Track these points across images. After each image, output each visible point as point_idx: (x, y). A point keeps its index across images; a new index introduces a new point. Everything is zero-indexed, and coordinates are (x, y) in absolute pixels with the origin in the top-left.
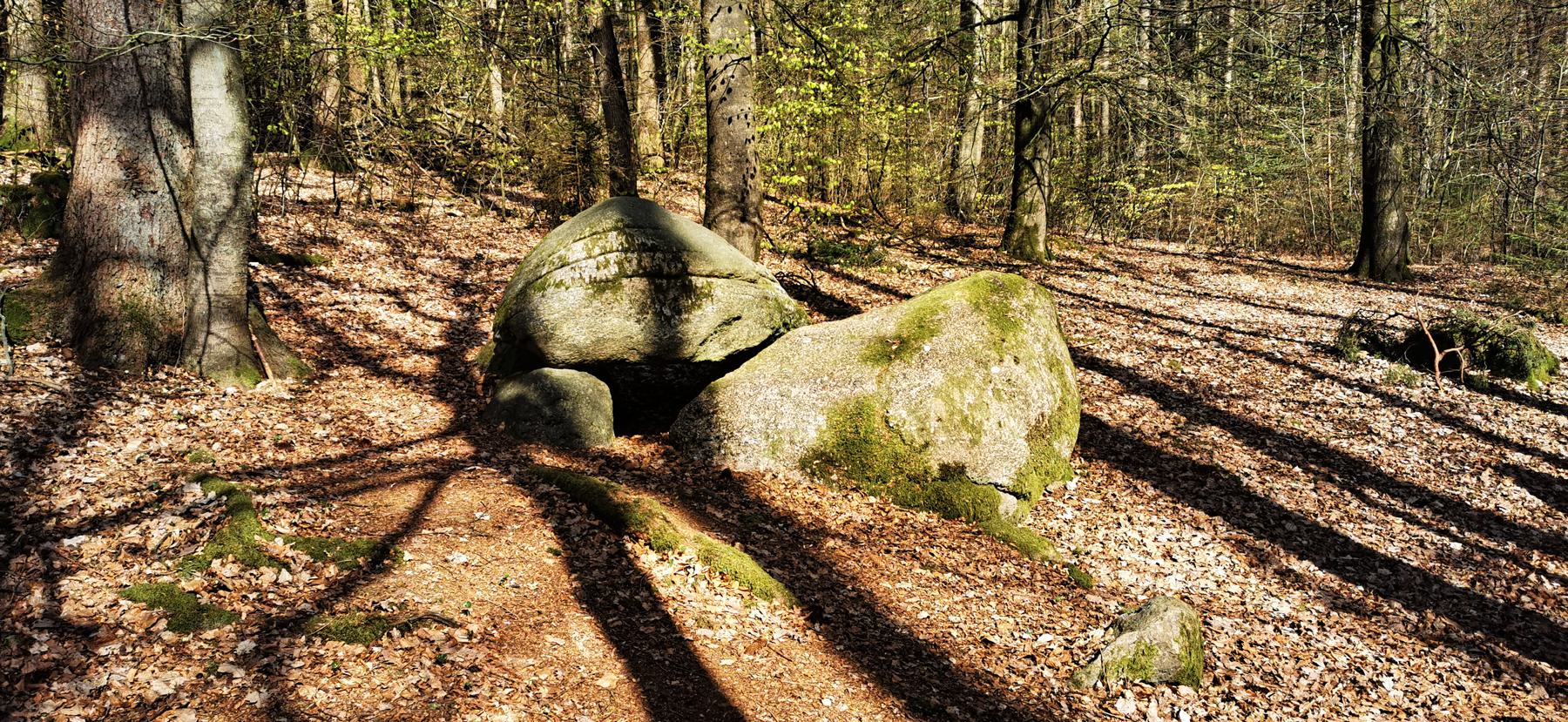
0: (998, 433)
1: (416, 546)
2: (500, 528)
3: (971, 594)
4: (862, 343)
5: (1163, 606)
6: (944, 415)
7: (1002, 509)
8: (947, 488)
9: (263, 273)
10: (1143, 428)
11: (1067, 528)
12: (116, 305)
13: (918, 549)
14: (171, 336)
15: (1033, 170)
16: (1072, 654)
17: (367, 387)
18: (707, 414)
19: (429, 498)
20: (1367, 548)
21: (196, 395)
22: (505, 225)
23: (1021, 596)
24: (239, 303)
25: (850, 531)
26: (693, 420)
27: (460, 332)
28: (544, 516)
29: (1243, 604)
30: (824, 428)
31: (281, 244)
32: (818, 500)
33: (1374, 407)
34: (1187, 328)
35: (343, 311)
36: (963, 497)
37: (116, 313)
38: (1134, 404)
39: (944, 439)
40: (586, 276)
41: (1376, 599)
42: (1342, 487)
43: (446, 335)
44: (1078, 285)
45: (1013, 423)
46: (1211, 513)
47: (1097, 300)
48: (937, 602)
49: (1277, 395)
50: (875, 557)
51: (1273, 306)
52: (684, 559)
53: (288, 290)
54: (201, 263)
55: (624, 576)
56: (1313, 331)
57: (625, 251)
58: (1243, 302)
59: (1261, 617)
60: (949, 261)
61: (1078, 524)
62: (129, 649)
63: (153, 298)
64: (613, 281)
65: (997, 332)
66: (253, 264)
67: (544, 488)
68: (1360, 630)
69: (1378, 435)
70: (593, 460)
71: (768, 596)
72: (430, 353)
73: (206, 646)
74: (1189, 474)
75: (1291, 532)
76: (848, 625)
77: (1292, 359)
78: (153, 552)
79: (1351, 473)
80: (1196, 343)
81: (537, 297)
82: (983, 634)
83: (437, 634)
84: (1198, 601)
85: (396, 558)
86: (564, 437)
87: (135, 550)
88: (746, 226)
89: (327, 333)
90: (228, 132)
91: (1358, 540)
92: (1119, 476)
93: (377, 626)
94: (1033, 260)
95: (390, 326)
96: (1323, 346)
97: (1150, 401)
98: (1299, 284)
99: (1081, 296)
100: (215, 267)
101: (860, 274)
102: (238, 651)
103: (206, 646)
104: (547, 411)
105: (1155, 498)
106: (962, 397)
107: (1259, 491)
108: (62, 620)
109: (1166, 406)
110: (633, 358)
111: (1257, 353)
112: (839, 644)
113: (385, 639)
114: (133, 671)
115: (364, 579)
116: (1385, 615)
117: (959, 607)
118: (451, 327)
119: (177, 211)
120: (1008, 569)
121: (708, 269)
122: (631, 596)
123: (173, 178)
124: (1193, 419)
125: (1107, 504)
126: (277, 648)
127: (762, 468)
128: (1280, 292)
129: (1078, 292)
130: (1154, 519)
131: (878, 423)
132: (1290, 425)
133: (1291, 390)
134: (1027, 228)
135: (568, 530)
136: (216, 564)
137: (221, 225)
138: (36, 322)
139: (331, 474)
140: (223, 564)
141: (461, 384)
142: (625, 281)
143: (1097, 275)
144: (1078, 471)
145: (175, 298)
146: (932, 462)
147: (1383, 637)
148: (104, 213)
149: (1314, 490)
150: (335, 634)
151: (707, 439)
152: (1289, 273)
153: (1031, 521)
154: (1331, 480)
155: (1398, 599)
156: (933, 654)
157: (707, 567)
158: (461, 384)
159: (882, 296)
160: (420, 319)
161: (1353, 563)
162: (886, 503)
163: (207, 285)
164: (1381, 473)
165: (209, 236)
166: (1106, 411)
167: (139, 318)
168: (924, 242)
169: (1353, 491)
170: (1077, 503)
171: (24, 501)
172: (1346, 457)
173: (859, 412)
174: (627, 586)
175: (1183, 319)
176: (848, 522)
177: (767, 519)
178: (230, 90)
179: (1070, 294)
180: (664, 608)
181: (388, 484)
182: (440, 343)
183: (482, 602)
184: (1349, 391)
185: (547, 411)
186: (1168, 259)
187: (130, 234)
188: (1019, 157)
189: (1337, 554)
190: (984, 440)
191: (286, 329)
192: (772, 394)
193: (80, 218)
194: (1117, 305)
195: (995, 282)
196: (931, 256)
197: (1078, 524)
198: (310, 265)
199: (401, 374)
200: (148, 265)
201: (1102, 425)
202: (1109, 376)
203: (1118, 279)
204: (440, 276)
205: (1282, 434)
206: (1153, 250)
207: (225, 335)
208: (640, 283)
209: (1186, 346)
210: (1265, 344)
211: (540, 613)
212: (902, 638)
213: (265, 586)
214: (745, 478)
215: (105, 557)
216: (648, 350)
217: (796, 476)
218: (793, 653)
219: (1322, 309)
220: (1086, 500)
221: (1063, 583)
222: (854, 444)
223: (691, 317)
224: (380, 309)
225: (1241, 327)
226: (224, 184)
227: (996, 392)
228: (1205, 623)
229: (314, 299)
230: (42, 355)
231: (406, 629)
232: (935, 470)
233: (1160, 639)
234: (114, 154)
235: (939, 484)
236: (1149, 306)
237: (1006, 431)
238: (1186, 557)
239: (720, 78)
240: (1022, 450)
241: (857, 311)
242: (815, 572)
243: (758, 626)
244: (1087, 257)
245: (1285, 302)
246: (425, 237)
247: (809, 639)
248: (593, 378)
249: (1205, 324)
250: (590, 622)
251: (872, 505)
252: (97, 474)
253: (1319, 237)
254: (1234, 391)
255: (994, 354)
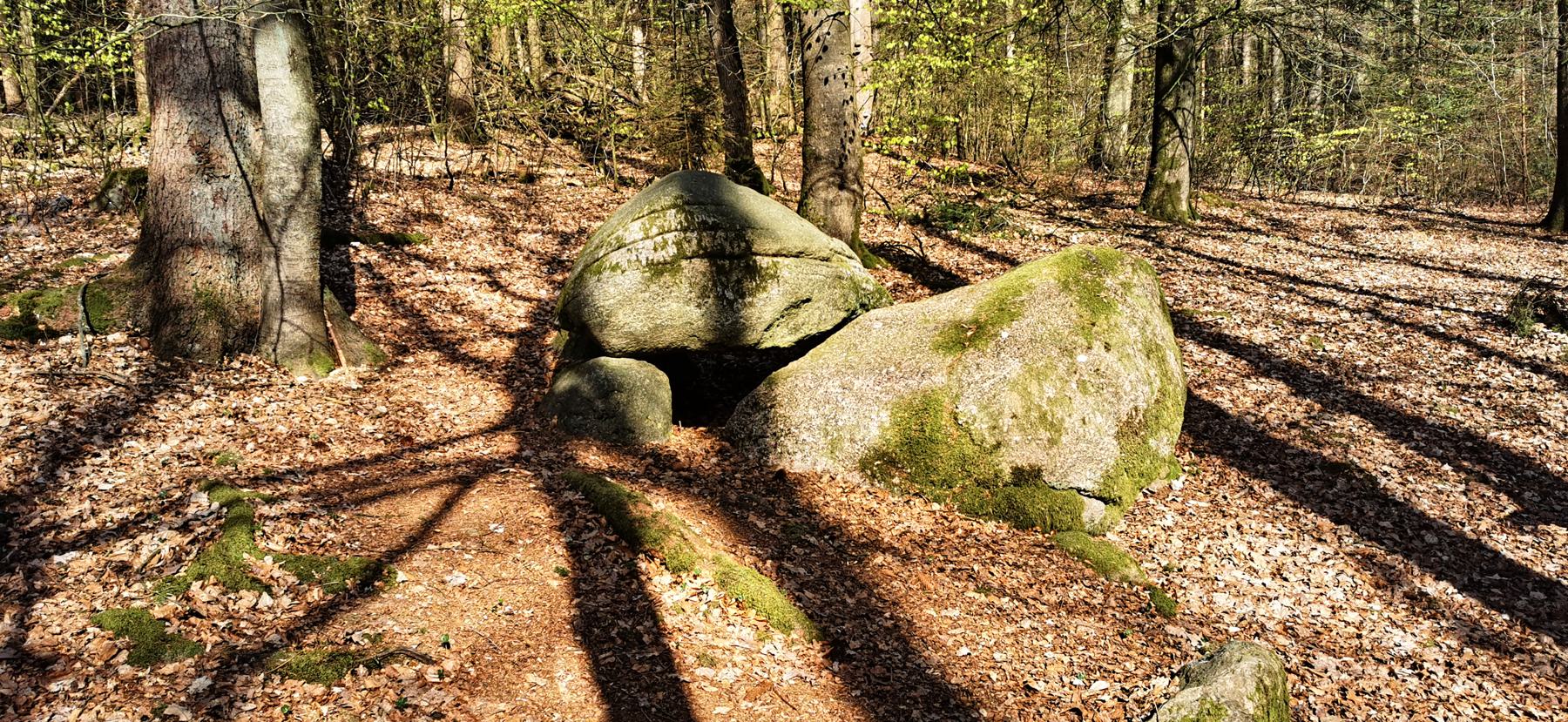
0: (1081, 430)
1: (415, 564)
2: (511, 543)
3: (1026, 624)
4: (936, 328)
5: (1237, 655)
6: (1020, 412)
7: (1085, 516)
8: (1019, 494)
9: (363, 254)
10: (1268, 416)
11: (1163, 536)
12: (191, 293)
13: (976, 568)
14: (247, 324)
15: (1175, 122)
16: (1125, 708)
17: (438, 374)
18: (764, 408)
19: (448, 506)
20: (1521, 566)
21: (262, 386)
22: (617, 196)
23: (1086, 627)
24: (312, 289)
25: (904, 545)
26: (750, 415)
27: (547, 312)
28: (561, 529)
29: (1359, 636)
30: (887, 425)
31: (386, 223)
32: (875, 505)
33: (1546, 391)
34: (1338, 296)
35: (434, 291)
36: (1037, 505)
37: (191, 301)
38: (1262, 388)
39: (1018, 438)
40: (643, 258)
41: (1523, 632)
42: (1498, 489)
43: (533, 317)
44: (1221, 247)
45: (1099, 419)
46: (1338, 521)
47: (1238, 265)
48: (984, 635)
49: (1433, 376)
50: (925, 579)
51: (1447, 269)
52: (698, 583)
53: (383, 271)
54: (272, 249)
55: (631, 601)
56: (1487, 298)
57: (685, 230)
58: (1412, 264)
59: (1378, 655)
60: (1079, 223)
61: (1178, 532)
62: (81, 685)
63: (229, 285)
64: (672, 263)
65: (1087, 314)
66: (353, 244)
67: (569, 495)
68: (1497, 672)
69: (1547, 425)
70: (641, 459)
71: (786, 628)
72: (511, 336)
73: (161, 682)
74: (1317, 472)
75: (1432, 545)
76: (872, 665)
77: (1456, 333)
78: (138, 572)
79: (1510, 472)
80: (1345, 315)
81: (592, 281)
82: (1028, 678)
83: (406, 671)
84: (1303, 632)
85: (389, 579)
86: (616, 432)
87: (123, 569)
88: (845, 194)
89: (414, 315)
90: (293, 113)
91: (1509, 555)
92: (1233, 475)
93: (343, 661)
94: (1174, 221)
95: (478, 307)
96: (1495, 317)
97: (1281, 385)
98: (1481, 240)
99: (1221, 260)
100: (286, 252)
101: (978, 241)
102: (191, 690)
103: (161, 682)
104: (600, 404)
105: (1273, 502)
106: (1042, 391)
107: (1399, 494)
108: (23, 650)
109: (1299, 391)
110: (694, 345)
111: (1416, 327)
112: (857, 688)
113: (348, 679)
114: (77, 711)
115: (348, 604)
116: (1531, 652)
117: (1008, 641)
118: (538, 308)
119: (251, 195)
120: (1077, 592)
121: (775, 248)
122: (633, 627)
123: (245, 162)
124: (1330, 406)
125: (1218, 509)
126: (231, 688)
127: (819, 469)
128: (1457, 250)
129: (1219, 256)
130: (1268, 528)
131: (945, 420)
132: (1444, 414)
133: (1451, 371)
134: (1167, 185)
135: (581, 546)
136: (196, 586)
137: (290, 210)
138: (116, 311)
139: (356, 478)
140: (203, 587)
141: (533, 371)
142: (684, 263)
143: (1244, 235)
144: (1186, 468)
145: (252, 285)
146: (1004, 464)
147: (1524, 682)
148: (177, 199)
149: (1464, 493)
150: (297, 672)
151: (763, 436)
152: (1470, 228)
153: (1124, 527)
154: (1485, 481)
155: (1550, 631)
156: (963, 703)
157: (723, 593)
158: (533, 371)
159: (997, 266)
160: (509, 299)
161: (1500, 585)
162: (951, 511)
163: (279, 271)
164: (1546, 472)
165: (279, 221)
166: (1228, 397)
167: (215, 307)
168: (1058, 202)
169: (1510, 494)
170: (1179, 506)
171: (31, 511)
172: (1506, 452)
173: (924, 407)
174: (631, 613)
175: (1337, 286)
176: (905, 533)
177: (813, 529)
178: (294, 69)
179: (1209, 258)
180: (666, 641)
181: (411, 489)
182: (523, 325)
183: (468, 632)
184: (1518, 372)
185: (600, 404)
186: (1332, 214)
187: (203, 221)
188: (1159, 108)
189: (1482, 573)
190: (1064, 439)
191: (373, 312)
192: (833, 387)
193: (156, 205)
194: (1260, 271)
195: (1088, 257)
196: (1062, 218)
197: (1178, 532)
198: (409, 243)
199: (475, 360)
200: (223, 252)
201: (1220, 413)
202: (1237, 355)
203: (1268, 240)
204: (538, 253)
205: (1433, 425)
206: (1317, 204)
207: (298, 322)
208: (700, 265)
209: (1333, 318)
210: (1427, 316)
211: (528, 646)
212: (932, 682)
213: (242, 611)
214: (800, 480)
215: (90, 577)
216: (709, 337)
217: (856, 478)
218: (801, 698)
219: (1503, 270)
220: (1192, 502)
221: (1140, 610)
222: (918, 443)
223: (755, 300)
224: (471, 289)
225: (1403, 295)
226: (291, 167)
227: (1082, 385)
228: (1306, 664)
229: (408, 280)
230: (120, 345)
231: (374, 666)
232: (1007, 475)
233: (1228, 697)
234: (186, 138)
235: (1008, 490)
236: (1299, 271)
237: (1091, 428)
238: (1300, 576)
239: (815, 36)
240: (1111, 450)
241: (965, 282)
242: (852, 595)
243: (768, 665)
244: (1237, 215)
245: (1460, 263)
246: (533, 210)
247: (823, 681)
248: (652, 367)
249: (1361, 291)
250: (580, 657)
251: (934, 512)
252: (120, 478)
253: (1513, 188)
254: (1383, 372)
255: (1082, 341)
